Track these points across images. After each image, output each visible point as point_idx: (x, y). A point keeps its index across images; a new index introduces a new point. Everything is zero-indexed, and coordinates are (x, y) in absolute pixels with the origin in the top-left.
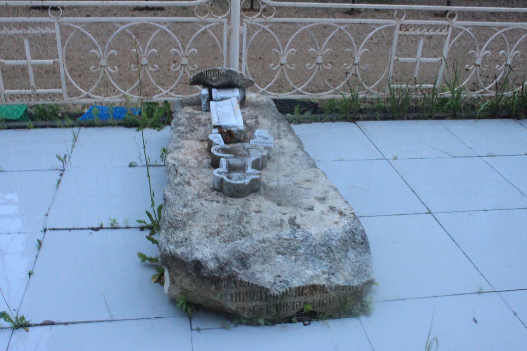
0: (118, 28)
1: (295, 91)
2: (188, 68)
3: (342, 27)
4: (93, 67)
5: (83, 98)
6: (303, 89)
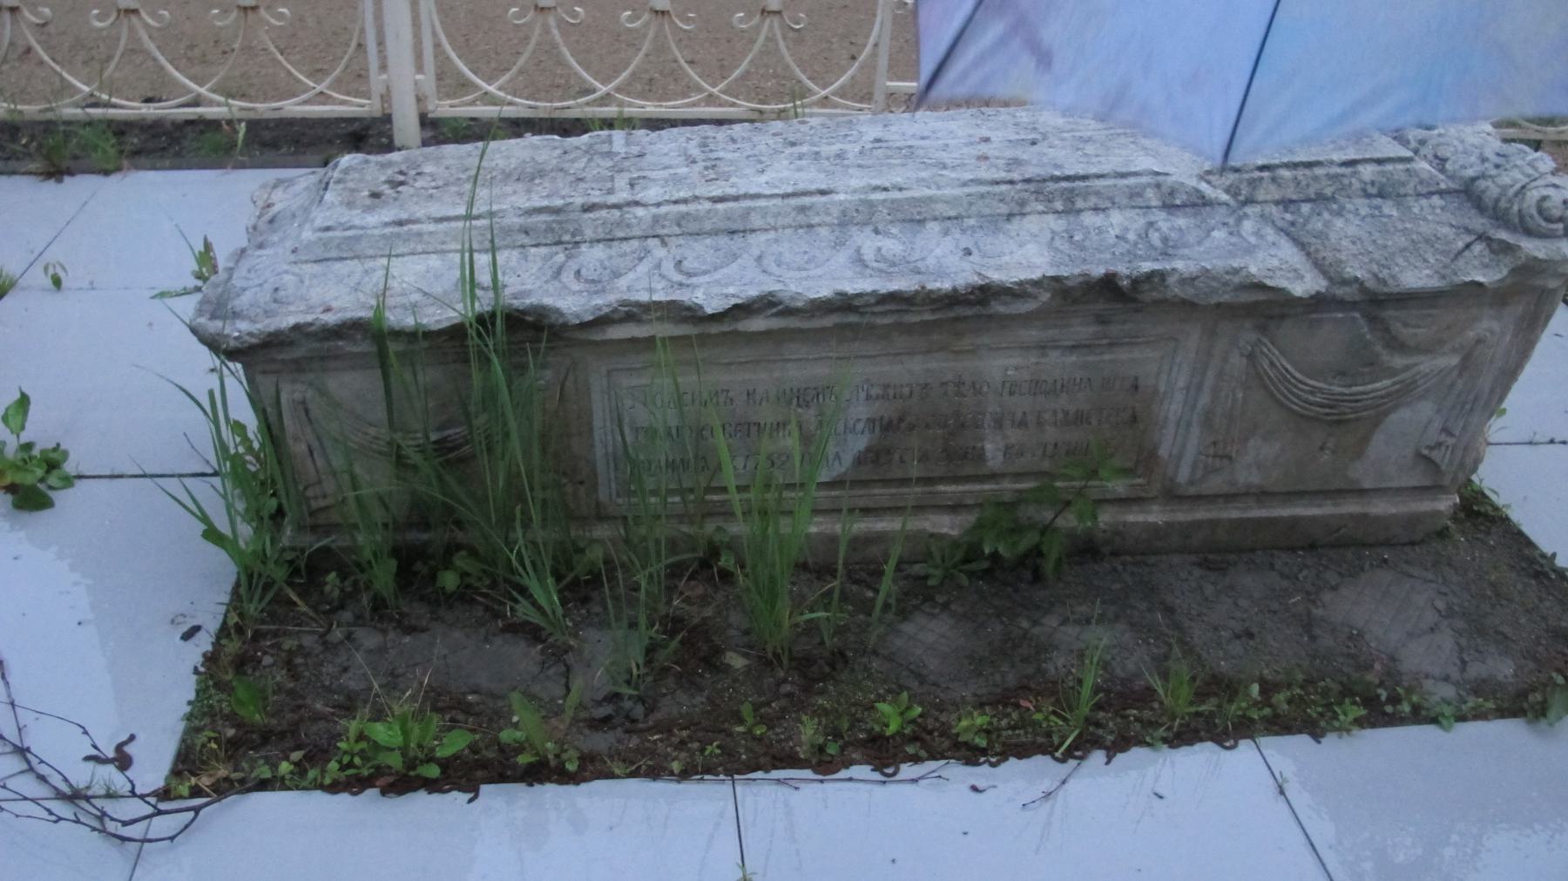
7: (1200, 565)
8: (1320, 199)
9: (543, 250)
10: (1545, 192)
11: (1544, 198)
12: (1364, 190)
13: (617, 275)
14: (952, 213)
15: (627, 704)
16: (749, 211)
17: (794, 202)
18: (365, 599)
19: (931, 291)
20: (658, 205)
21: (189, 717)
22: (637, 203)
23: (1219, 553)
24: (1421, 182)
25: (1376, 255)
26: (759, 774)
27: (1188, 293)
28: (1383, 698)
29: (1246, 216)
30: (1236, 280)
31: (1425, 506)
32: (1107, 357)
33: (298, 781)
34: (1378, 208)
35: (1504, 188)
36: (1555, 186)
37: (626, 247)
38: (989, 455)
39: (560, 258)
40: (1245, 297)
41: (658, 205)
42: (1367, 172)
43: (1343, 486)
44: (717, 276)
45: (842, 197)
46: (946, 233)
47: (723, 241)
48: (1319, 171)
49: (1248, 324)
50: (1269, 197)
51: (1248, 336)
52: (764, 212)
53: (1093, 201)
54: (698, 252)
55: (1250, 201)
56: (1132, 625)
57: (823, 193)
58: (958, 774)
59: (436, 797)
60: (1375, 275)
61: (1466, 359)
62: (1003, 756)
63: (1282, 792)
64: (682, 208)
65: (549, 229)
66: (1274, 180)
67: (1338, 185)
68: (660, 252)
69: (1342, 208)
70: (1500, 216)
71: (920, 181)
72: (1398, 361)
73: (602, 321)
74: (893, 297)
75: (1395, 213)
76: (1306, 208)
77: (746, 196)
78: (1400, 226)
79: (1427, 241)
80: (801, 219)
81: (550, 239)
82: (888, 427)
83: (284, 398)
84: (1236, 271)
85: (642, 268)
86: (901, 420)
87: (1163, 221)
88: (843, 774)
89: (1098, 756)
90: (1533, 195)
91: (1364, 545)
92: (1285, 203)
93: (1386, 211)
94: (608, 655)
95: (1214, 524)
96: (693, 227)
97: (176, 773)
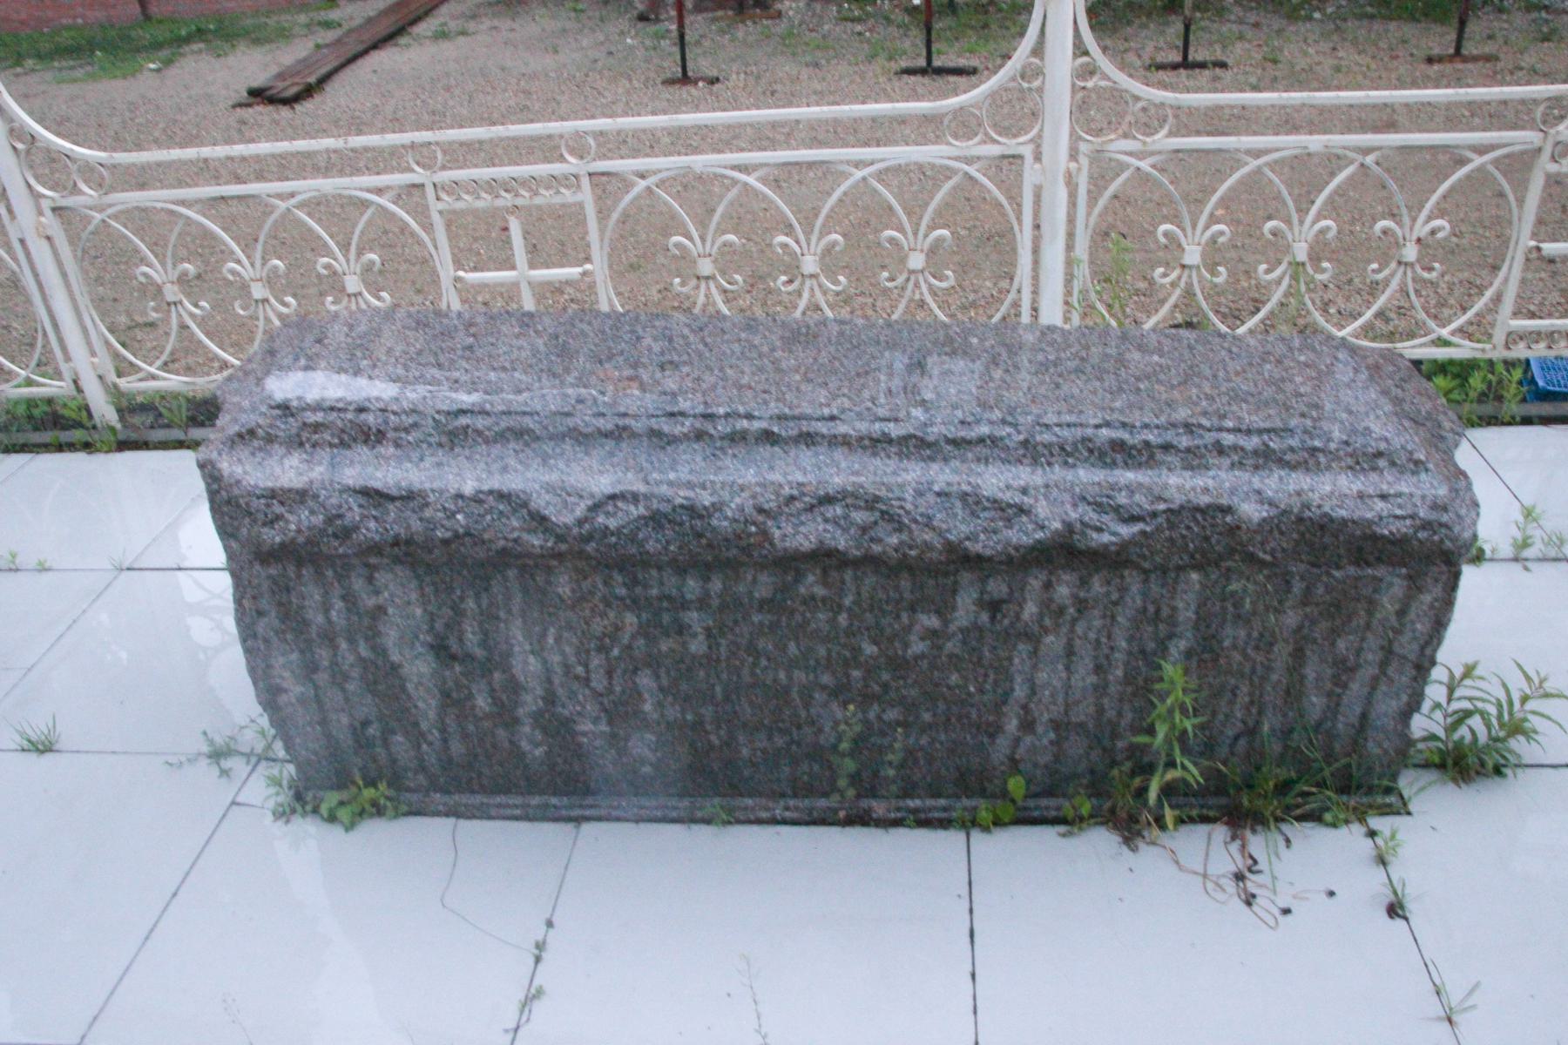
1: (1429, 338)
3: (1370, 160)
5: (19, 386)
6: (1453, 333)
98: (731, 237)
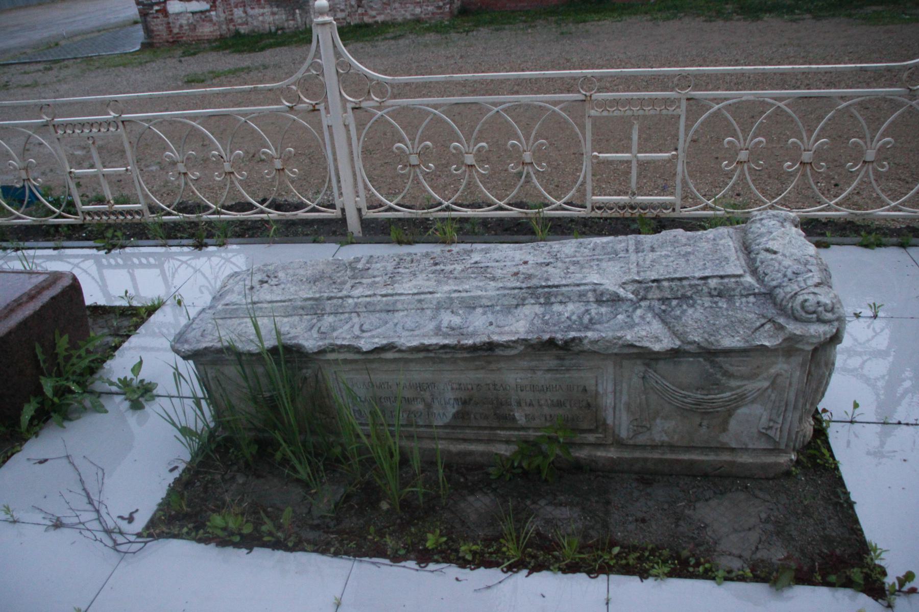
0: (711, 107)
2: (477, 171)
4: (455, 166)
7: (637, 480)
8: (684, 298)
9: (309, 317)
10: (806, 297)
11: (806, 301)
12: (710, 293)
13: (334, 330)
14: (489, 304)
15: (328, 520)
16: (396, 301)
17: (417, 297)
18: (241, 461)
19: (463, 345)
20: (358, 298)
21: (160, 505)
22: (349, 297)
23: (647, 476)
24: (744, 289)
25: (707, 330)
26: (367, 559)
27: (596, 348)
28: (692, 563)
29: (640, 307)
30: (620, 342)
31: (771, 459)
32: (567, 375)
33: (187, 536)
34: (716, 303)
35: (786, 293)
36: (814, 293)
37: (342, 317)
38: (518, 418)
39: (315, 321)
40: (626, 351)
41: (358, 298)
42: (713, 283)
43: (718, 445)
44: (374, 333)
45: (438, 295)
46: (484, 313)
47: (383, 315)
48: (685, 283)
49: (639, 362)
50: (655, 297)
51: (639, 368)
52: (403, 302)
53: (560, 298)
54: (370, 320)
55: (644, 298)
56: (583, 509)
57: (431, 293)
58: (453, 571)
59: (236, 550)
60: (706, 340)
61: (773, 383)
62: (478, 566)
63: (607, 604)
64: (368, 299)
65: (312, 308)
66: (658, 287)
67: (695, 290)
68: (355, 319)
69: (695, 302)
70: (782, 310)
71: (478, 287)
72: (733, 383)
73: (322, 352)
74: (444, 347)
75: (725, 306)
76: (674, 303)
77: (396, 294)
78: (725, 313)
79: (740, 322)
80: (419, 305)
81: (312, 311)
82: (465, 403)
83: (209, 375)
84: (620, 338)
85: (347, 327)
86: (471, 399)
87: (594, 309)
88: (403, 564)
89: (525, 572)
90: (800, 298)
91: (738, 477)
92: (663, 300)
93: (720, 304)
94: (327, 497)
95: (645, 460)
96: (372, 308)
97: (147, 527)
98: (428, 143)
